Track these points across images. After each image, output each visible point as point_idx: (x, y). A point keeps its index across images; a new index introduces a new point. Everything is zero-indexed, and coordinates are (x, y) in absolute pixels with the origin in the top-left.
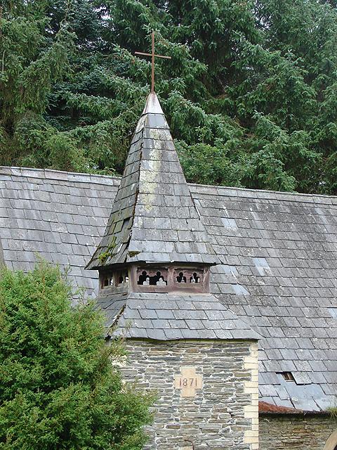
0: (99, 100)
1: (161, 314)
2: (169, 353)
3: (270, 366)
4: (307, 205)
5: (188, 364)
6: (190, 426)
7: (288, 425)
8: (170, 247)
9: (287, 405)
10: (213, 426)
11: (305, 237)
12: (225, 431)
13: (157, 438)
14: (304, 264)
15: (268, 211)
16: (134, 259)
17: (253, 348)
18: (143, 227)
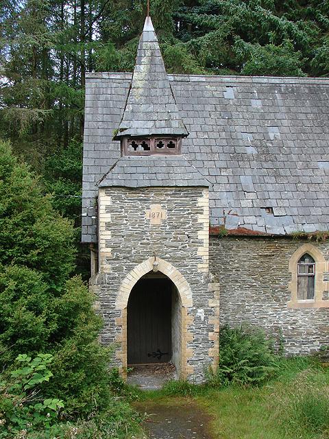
0: (215, 17)
1: (140, 170)
2: (142, 196)
3: (258, 203)
4: (324, 86)
5: (156, 203)
6: (157, 244)
7: (262, 243)
8: (151, 124)
9: (262, 230)
10: (174, 244)
11: (315, 110)
12: (183, 247)
13: (133, 251)
14: (308, 130)
15: (292, 92)
16: (123, 134)
17: (205, 192)
18: (132, 111)
